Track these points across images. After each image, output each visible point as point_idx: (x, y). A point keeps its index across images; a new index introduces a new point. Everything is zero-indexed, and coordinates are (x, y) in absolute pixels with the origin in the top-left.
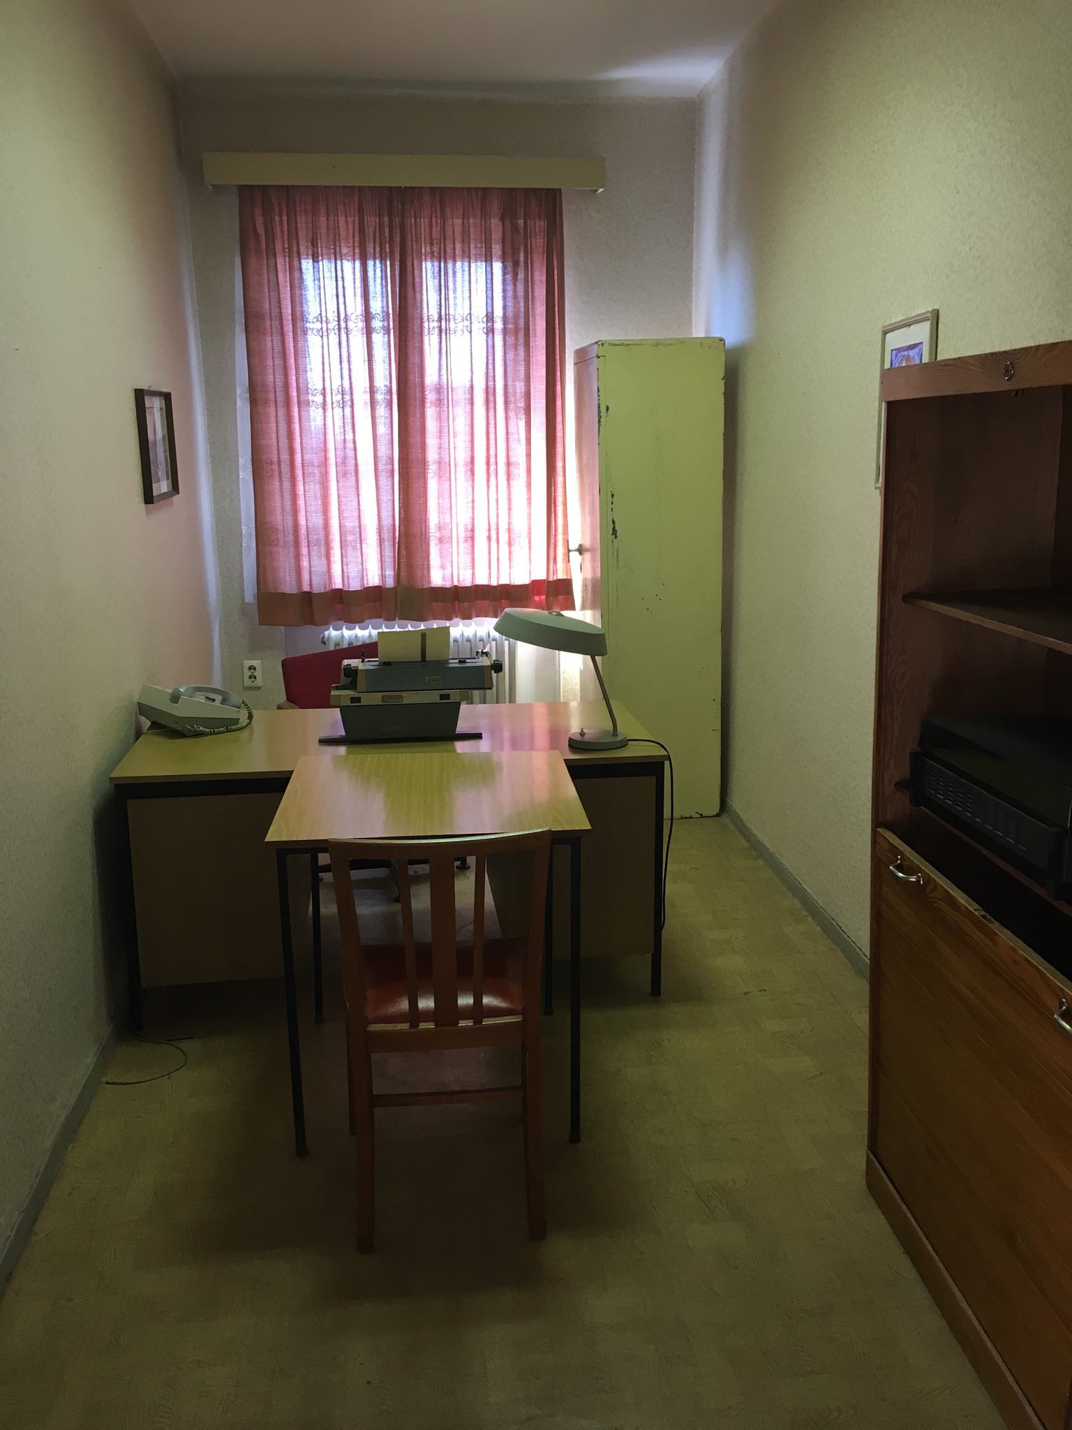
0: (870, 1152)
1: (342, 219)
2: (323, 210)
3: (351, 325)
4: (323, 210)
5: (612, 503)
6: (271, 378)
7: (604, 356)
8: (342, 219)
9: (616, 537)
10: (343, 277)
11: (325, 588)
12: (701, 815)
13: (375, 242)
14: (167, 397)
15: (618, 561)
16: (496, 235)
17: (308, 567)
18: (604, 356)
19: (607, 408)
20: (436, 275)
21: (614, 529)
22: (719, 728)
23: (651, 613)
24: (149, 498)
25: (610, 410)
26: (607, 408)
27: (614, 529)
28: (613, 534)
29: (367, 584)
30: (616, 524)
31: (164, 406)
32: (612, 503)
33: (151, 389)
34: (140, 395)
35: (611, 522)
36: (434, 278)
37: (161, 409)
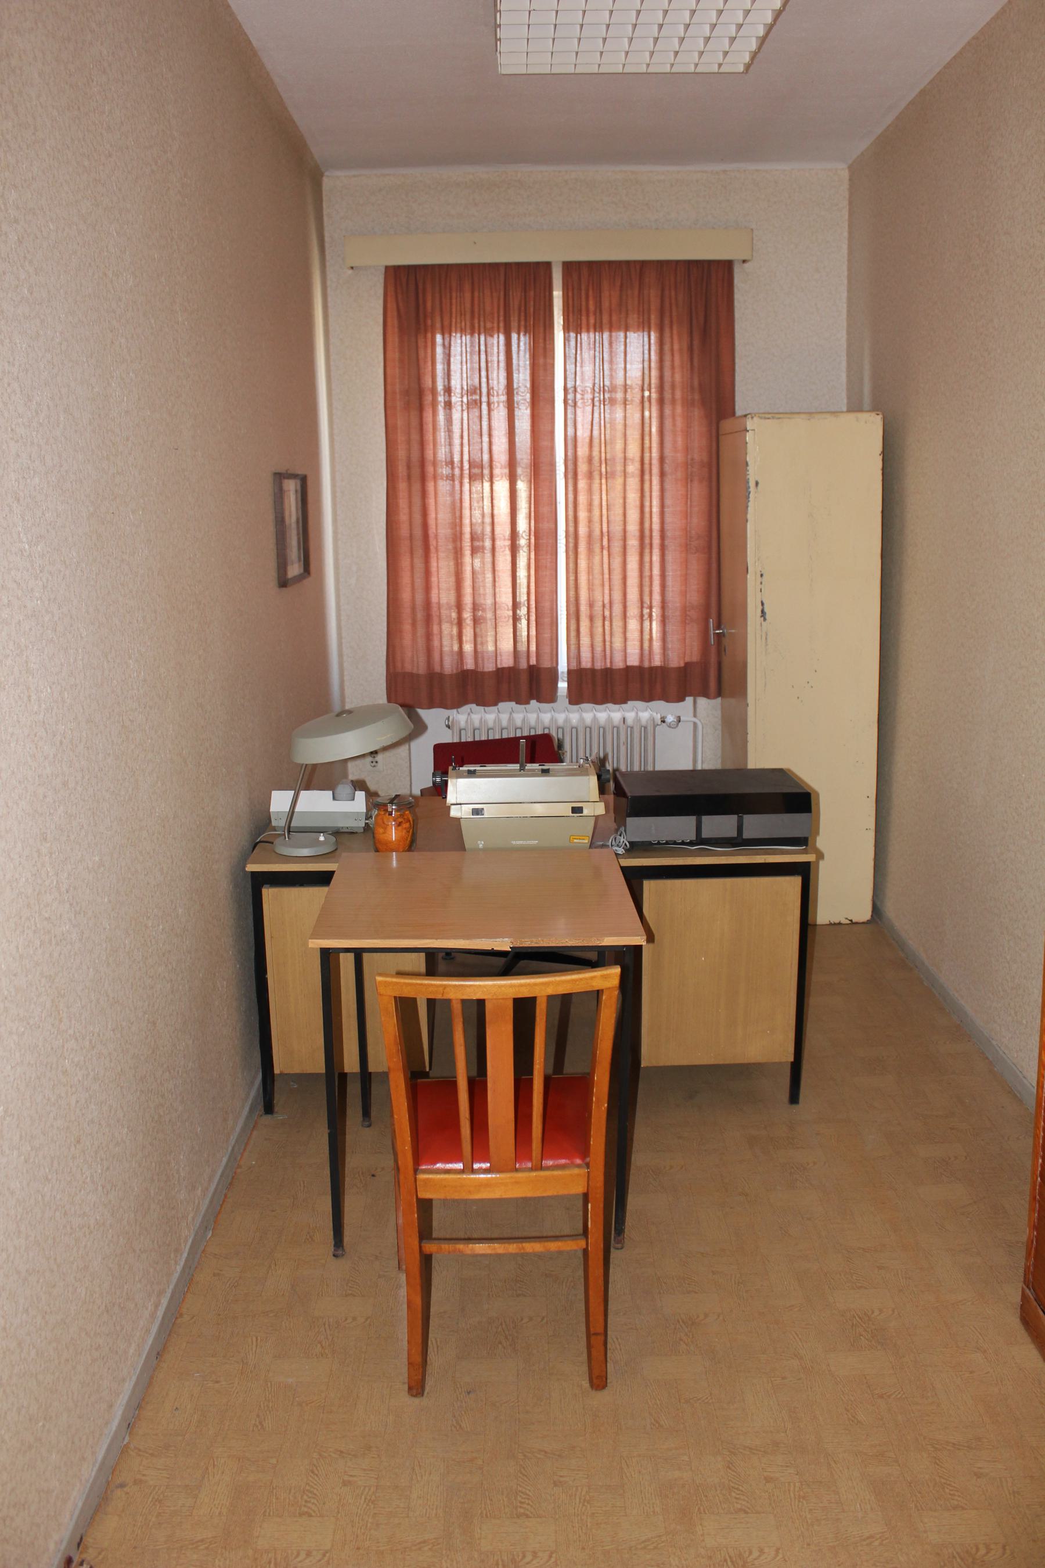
0: (1025, 1287)
1: (487, 292)
2: (467, 287)
3: (494, 399)
4: (467, 287)
5: (761, 583)
6: (678, 377)
7: (754, 430)
8: (487, 292)
9: (765, 620)
10: (486, 352)
11: (457, 669)
12: (851, 921)
13: (519, 321)
14: (590, 728)
15: (766, 645)
16: (655, 305)
17: (439, 647)
18: (754, 430)
19: (757, 484)
20: (592, 346)
21: (763, 611)
22: (873, 827)
23: (802, 701)
24: (283, 583)
25: (759, 485)
26: (757, 484)
27: (763, 611)
28: (762, 616)
29: (501, 664)
30: (765, 606)
31: (299, 488)
32: (761, 583)
33: (289, 472)
34: (280, 477)
35: (760, 604)
36: (590, 349)
37: (296, 491)
